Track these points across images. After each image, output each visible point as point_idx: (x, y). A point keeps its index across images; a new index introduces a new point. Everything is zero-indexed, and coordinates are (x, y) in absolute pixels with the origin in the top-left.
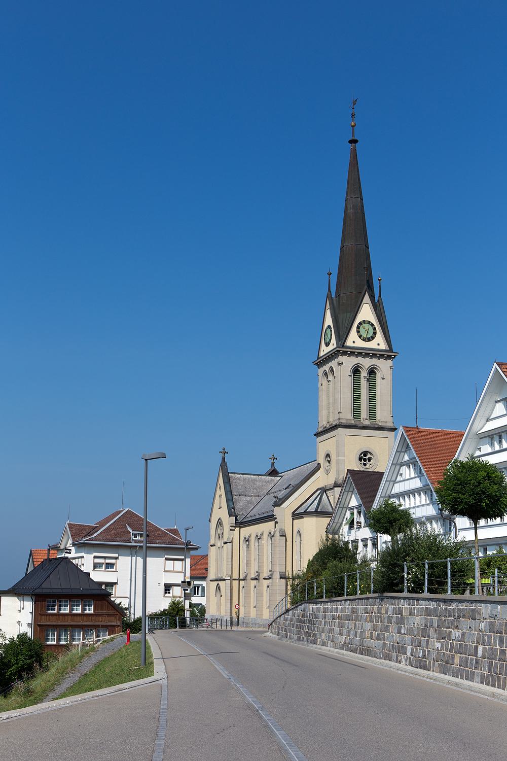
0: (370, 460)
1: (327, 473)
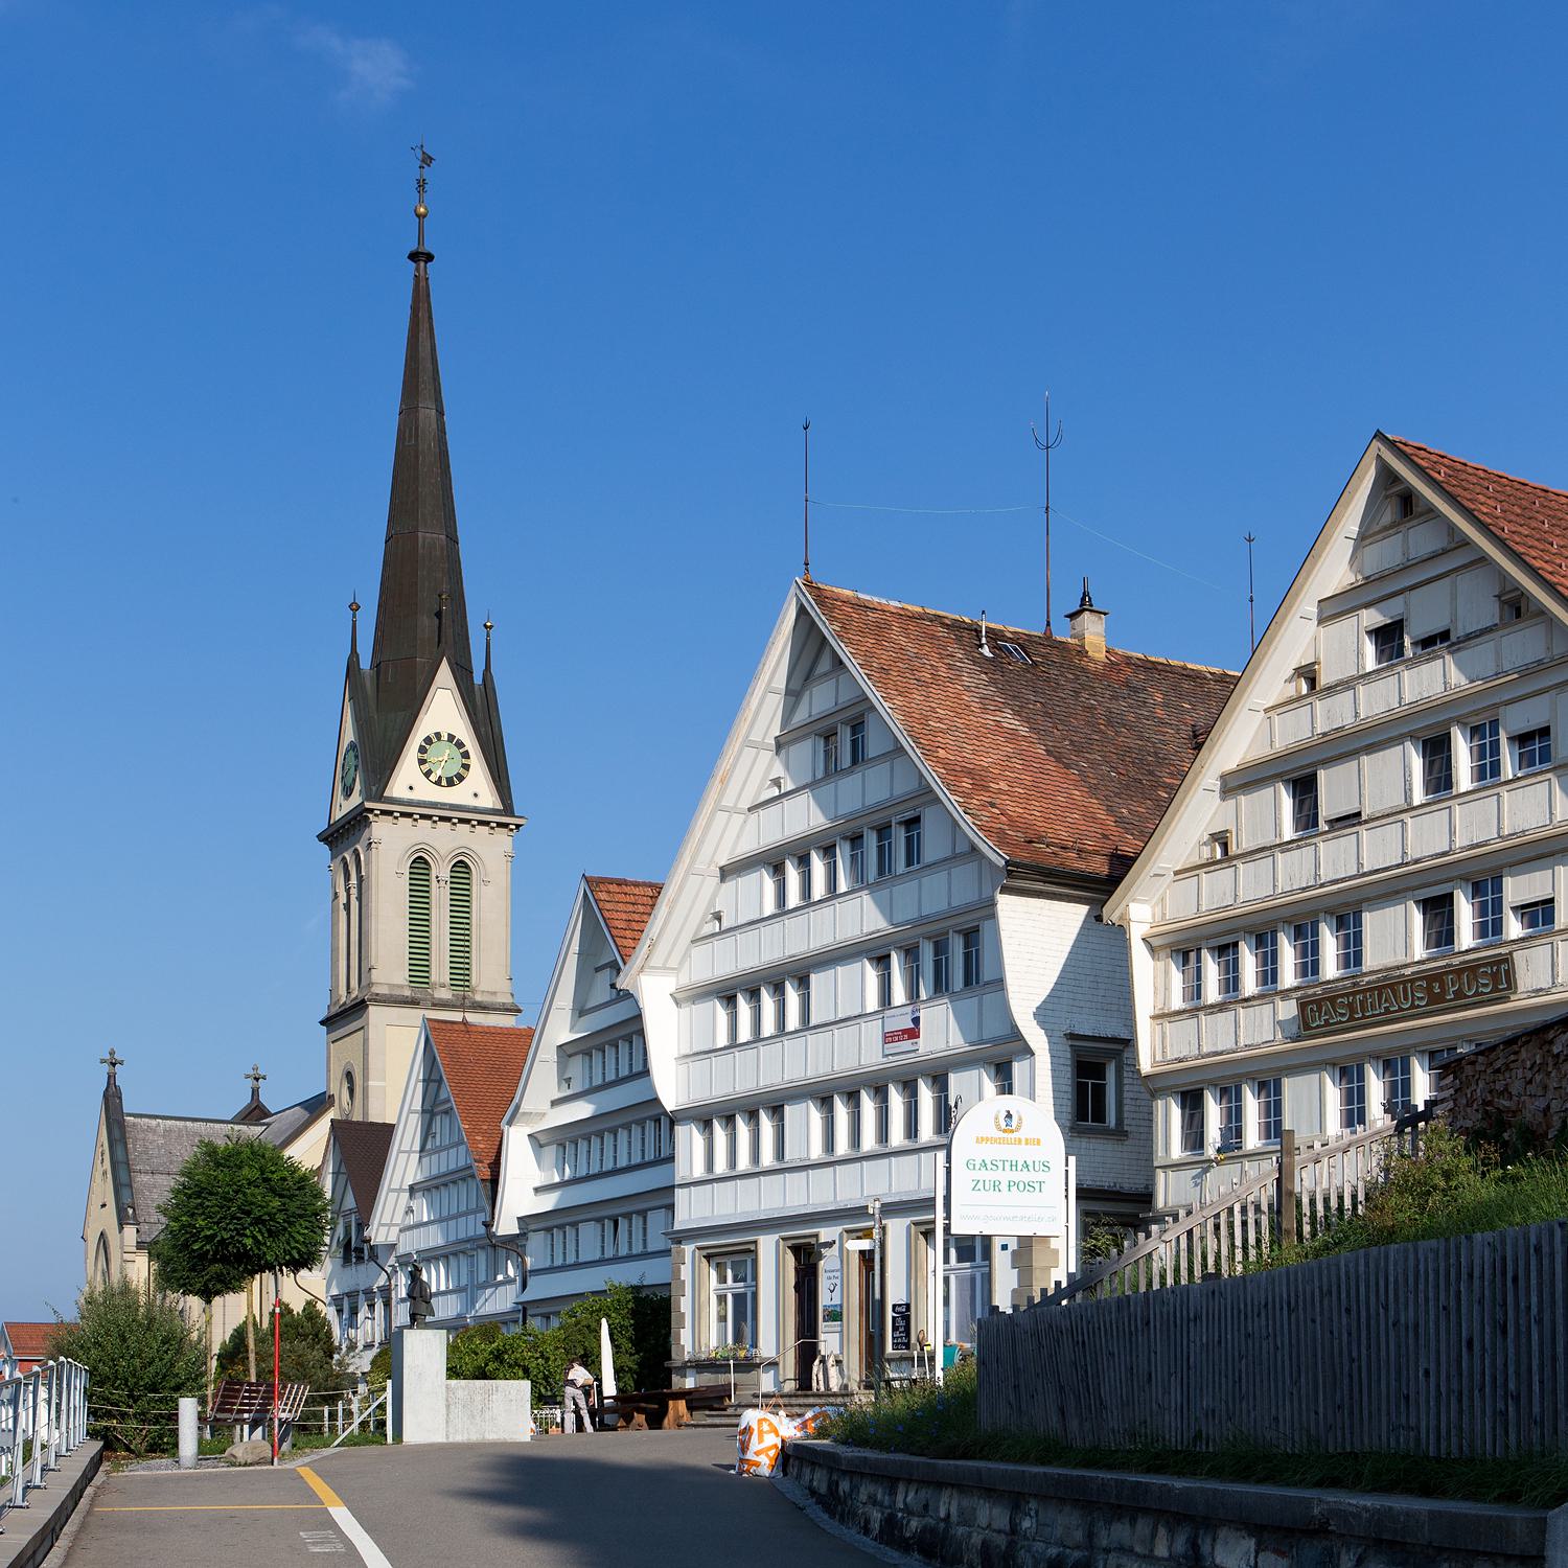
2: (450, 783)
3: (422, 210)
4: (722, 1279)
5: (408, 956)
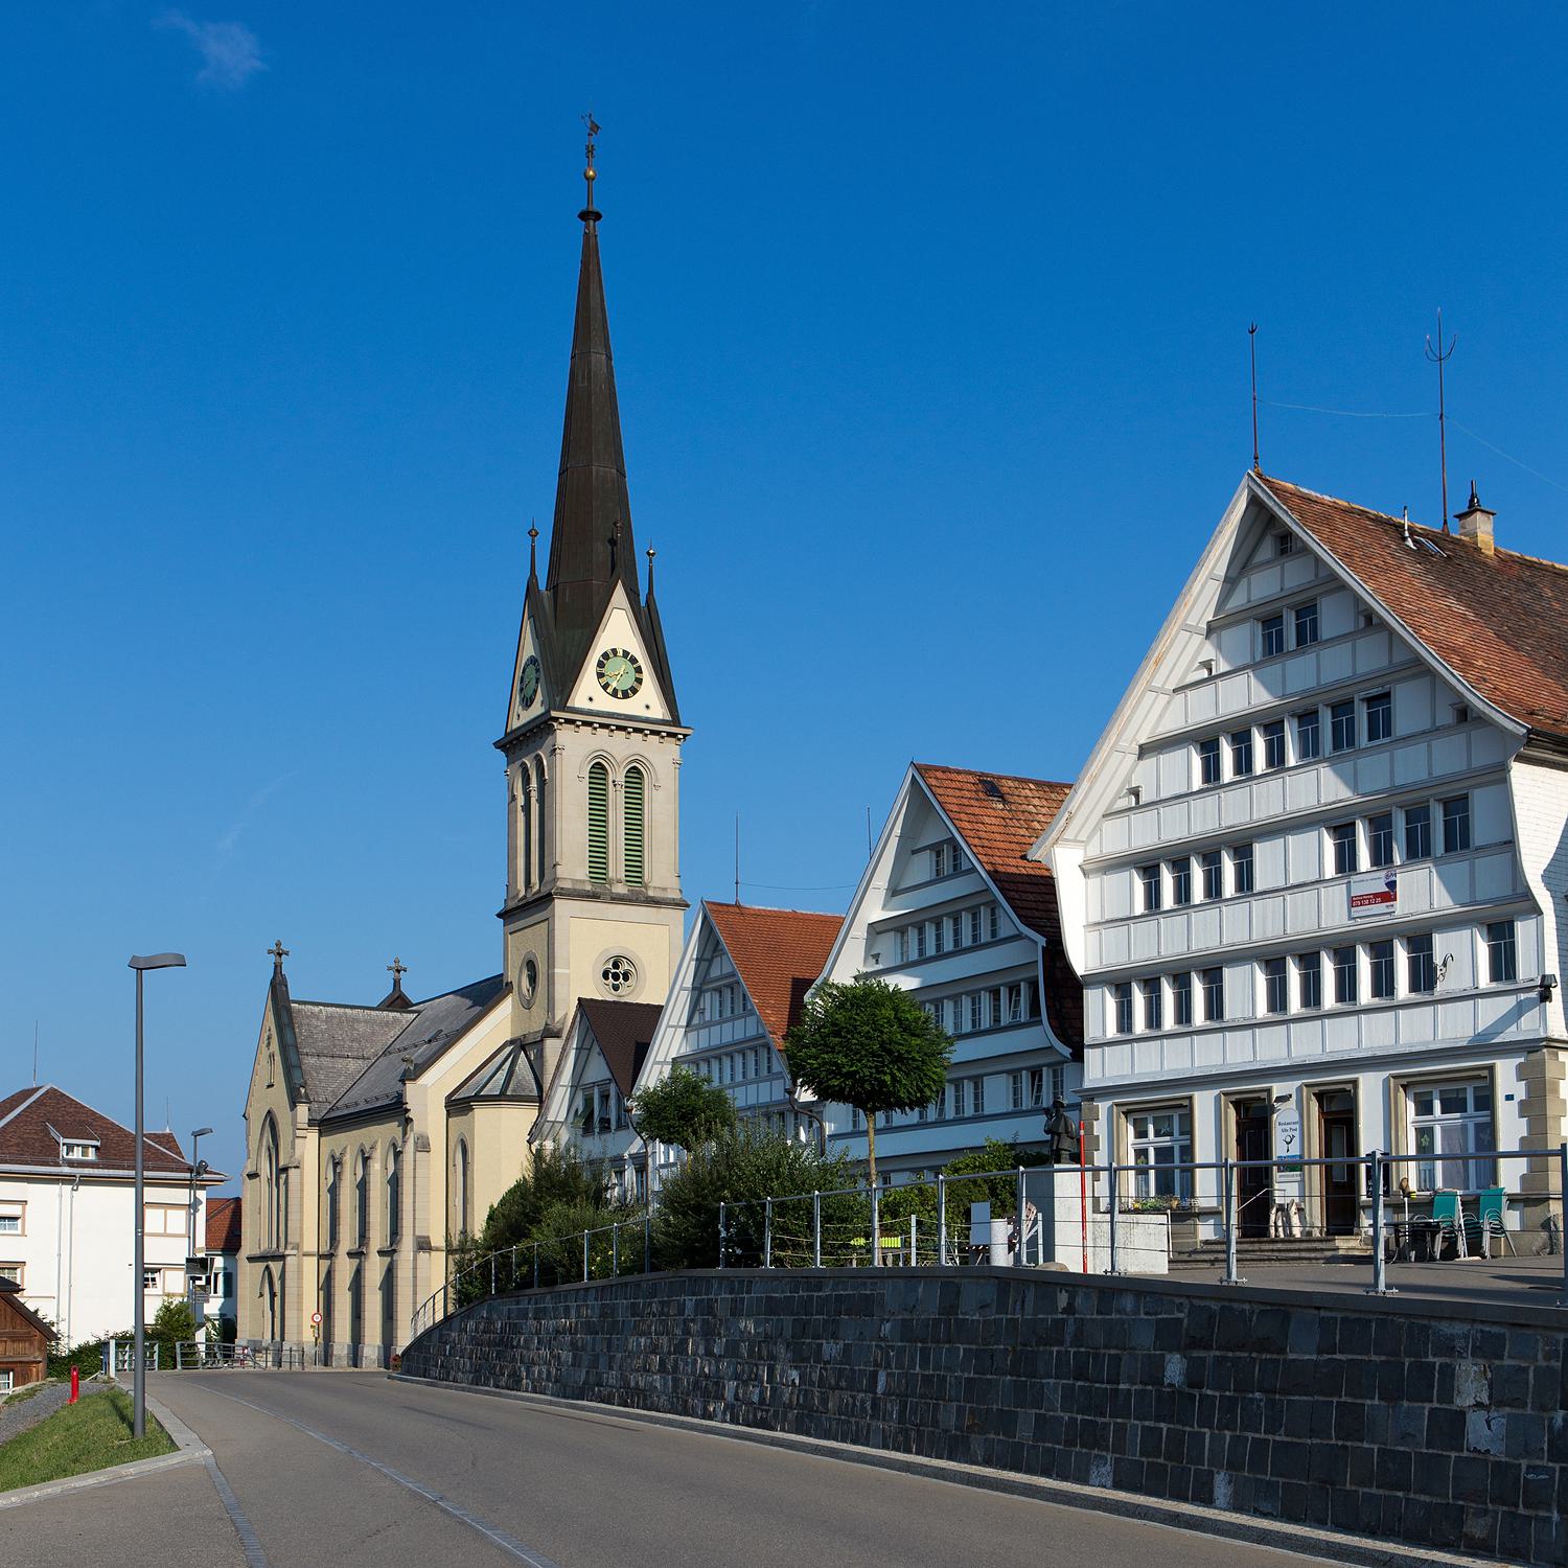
0: (626, 977)
1: (528, 1005)
2: (626, 695)
3: (591, 173)
4: (1141, 1133)
5: (588, 854)
